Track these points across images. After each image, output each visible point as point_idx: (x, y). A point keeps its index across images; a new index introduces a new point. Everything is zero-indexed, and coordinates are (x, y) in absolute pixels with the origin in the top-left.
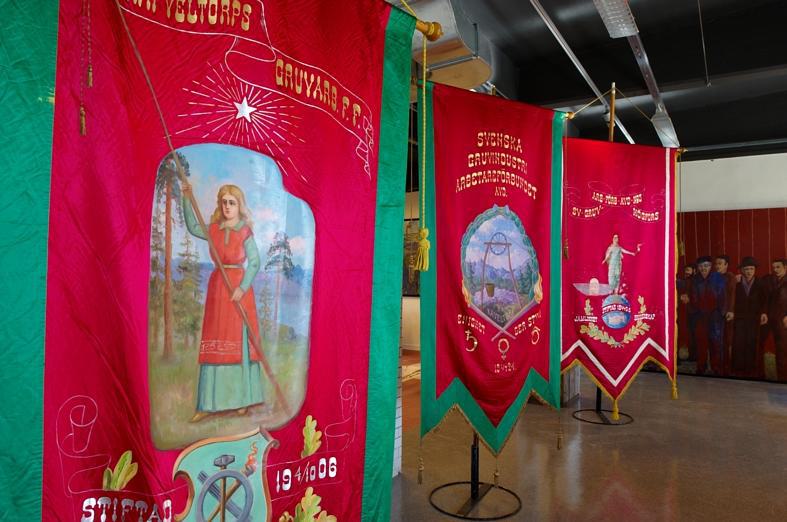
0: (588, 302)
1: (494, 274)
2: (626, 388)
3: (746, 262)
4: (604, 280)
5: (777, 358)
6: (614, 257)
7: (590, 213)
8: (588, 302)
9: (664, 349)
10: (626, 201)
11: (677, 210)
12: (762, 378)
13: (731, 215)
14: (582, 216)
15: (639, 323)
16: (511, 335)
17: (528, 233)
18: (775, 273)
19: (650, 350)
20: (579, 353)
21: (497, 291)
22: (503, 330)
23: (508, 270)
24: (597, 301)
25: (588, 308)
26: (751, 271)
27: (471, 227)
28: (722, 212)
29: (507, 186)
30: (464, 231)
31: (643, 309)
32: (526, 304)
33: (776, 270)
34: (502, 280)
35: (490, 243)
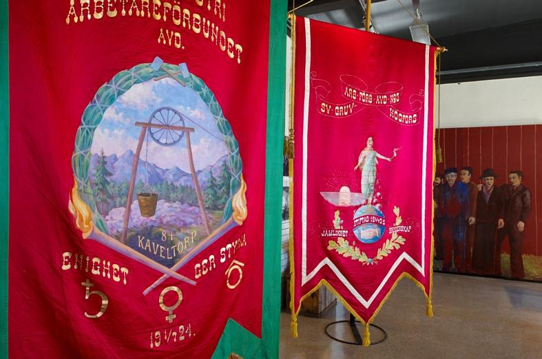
0: (337, 213)
1: (157, 176)
2: (378, 310)
3: (487, 173)
4: (356, 188)
5: (511, 258)
6: (368, 161)
7: (340, 111)
8: (337, 213)
9: (420, 264)
10: (382, 99)
11: (435, 126)
12: (498, 275)
13: (475, 131)
14: (333, 112)
15: (394, 236)
16: (186, 279)
17: (226, 114)
18: (511, 184)
19: (405, 266)
20: (326, 272)
21: (163, 207)
22: (171, 272)
23: (188, 171)
24: (347, 213)
25: (337, 221)
26: (490, 181)
27: (103, 91)
28: (467, 128)
29: (186, 33)
30: (89, 97)
31: (399, 221)
32: (217, 224)
33: (512, 180)
34: (174, 188)
35: (147, 126)
